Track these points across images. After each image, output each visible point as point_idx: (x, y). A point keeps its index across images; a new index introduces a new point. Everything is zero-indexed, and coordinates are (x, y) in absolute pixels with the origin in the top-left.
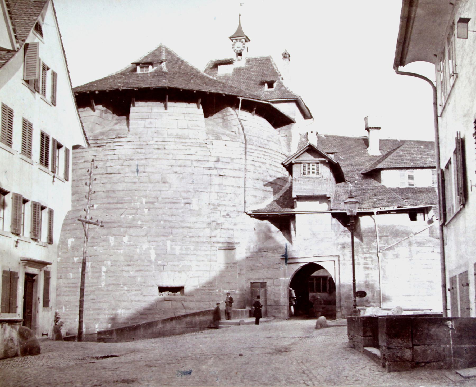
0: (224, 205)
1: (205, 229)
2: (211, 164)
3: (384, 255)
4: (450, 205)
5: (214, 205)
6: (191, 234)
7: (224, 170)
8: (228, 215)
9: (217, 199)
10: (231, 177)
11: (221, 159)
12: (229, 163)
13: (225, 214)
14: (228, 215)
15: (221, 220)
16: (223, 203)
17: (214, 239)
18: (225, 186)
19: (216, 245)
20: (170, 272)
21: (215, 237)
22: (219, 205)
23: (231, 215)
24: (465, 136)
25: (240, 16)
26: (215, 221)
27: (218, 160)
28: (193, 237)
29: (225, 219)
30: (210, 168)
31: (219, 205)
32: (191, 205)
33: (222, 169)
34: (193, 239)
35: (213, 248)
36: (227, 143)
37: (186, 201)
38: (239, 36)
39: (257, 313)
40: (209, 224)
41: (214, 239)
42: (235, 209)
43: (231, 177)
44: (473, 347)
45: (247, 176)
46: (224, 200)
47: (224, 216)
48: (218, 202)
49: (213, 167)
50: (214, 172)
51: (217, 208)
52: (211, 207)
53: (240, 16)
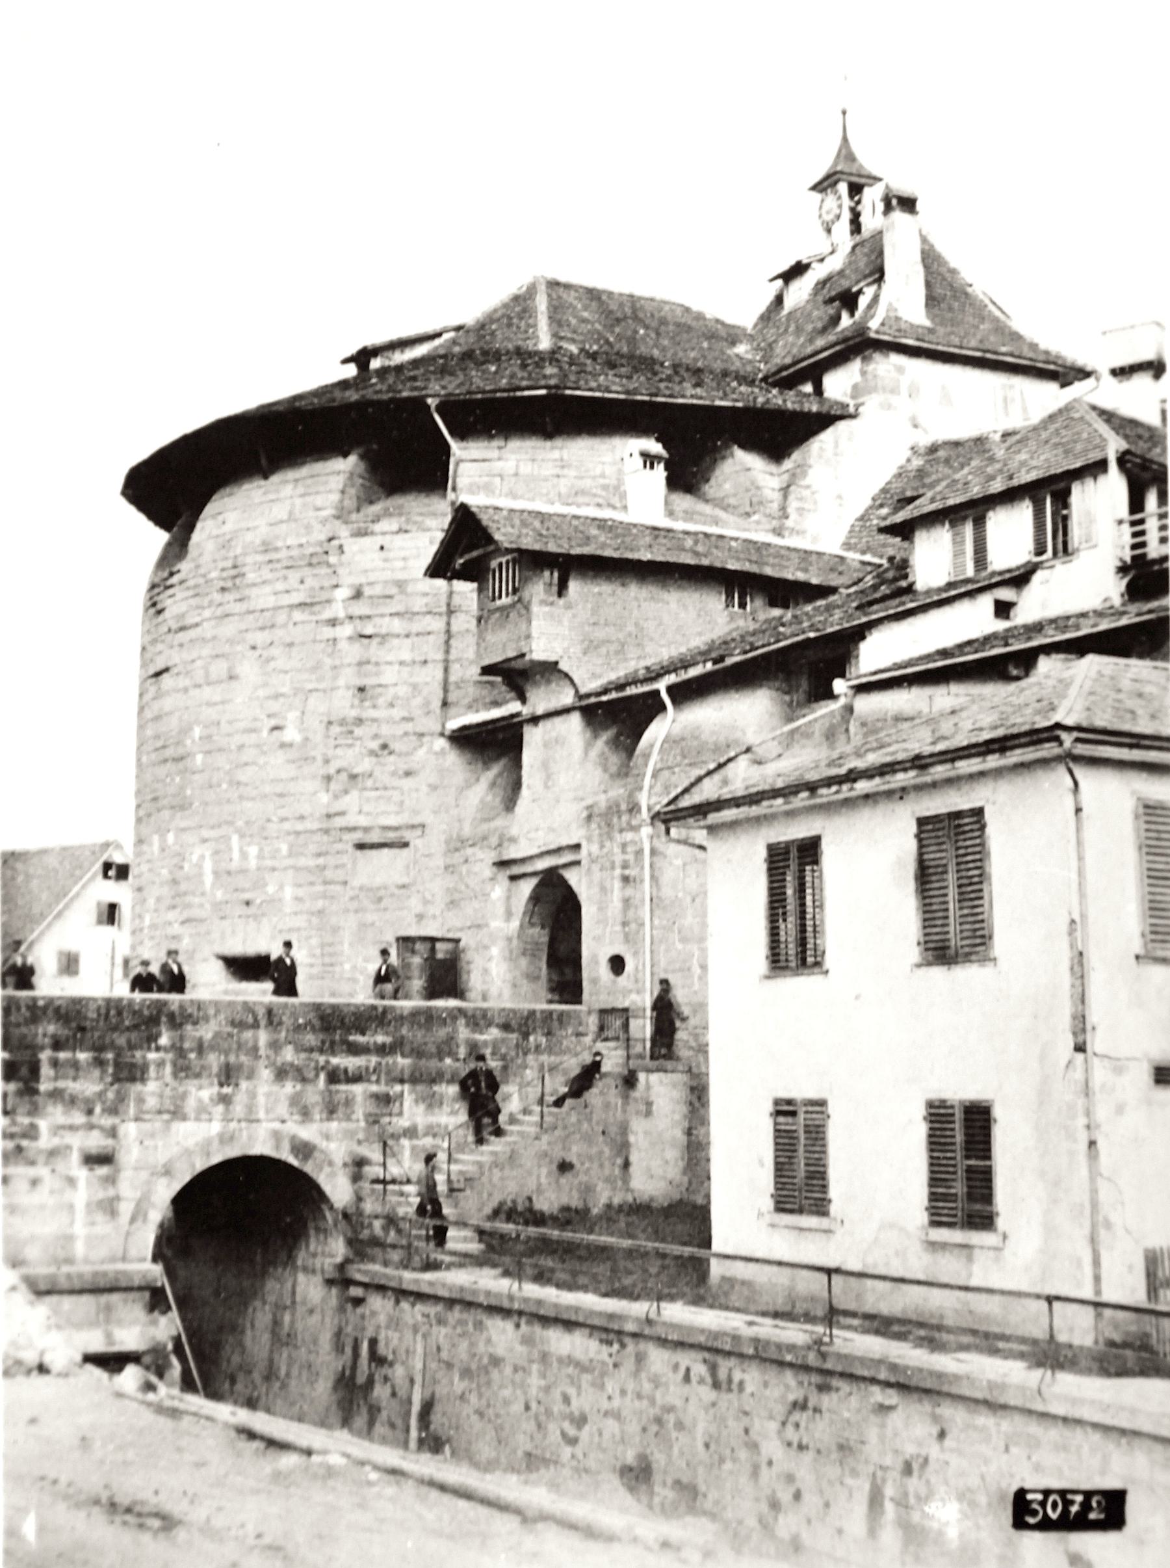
0: (374, 720)
1: (315, 793)
2: (338, 610)
5: (343, 722)
6: (283, 813)
7: (377, 620)
8: (384, 746)
11: (367, 591)
12: (390, 597)
13: (375, 745)
14: (384, 746)
15: (365, 765)
16: (372, 713)
17: (339, 822)
18: (377, 664)
20: (236, 920)
21: (342, 814)
22: (359, 721)
24: (346, 361)
25: (844, 113)
27: (358, 595)
29: (374, 759)
30: (333, 622)
31: (359, 721)
32: (286, 732)
33: (369, 617)
34: (287, 826)
36: (386, 540)
37: (273, 722)
38: (846, 180)
39: (1088, 1127)
41: (339, 822)
42: (409, 727)
44: (363, 1034)
45: (454, 628)
47: (373, 753)
50: (347, 630)
51: (351, 732)
52: (336, 729)
53: (844, 113)
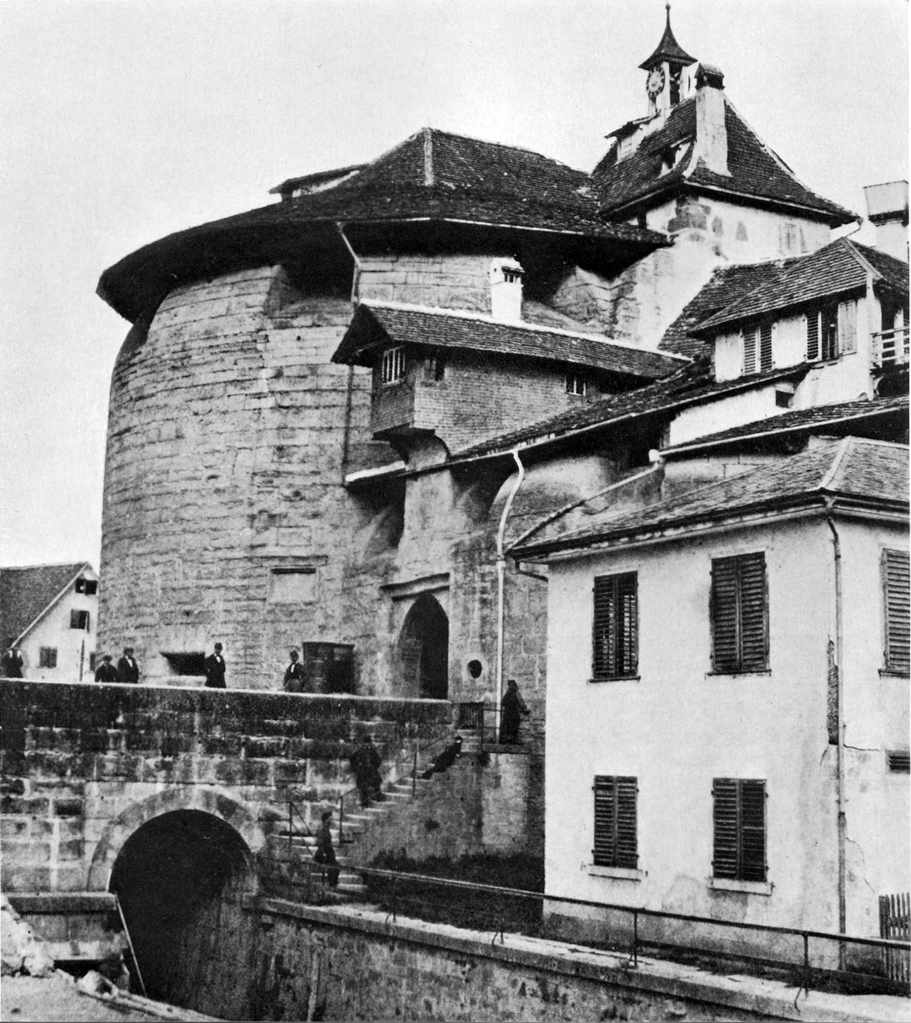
3: (336, 666)
4: (575, 351)
5: (264, 474)
8: (297, 494)
9: (273, 461)
10: (310, 407)
11: (286, 372)
13: (288, 492)
14: (297, 494)
17: (260, 552)
18: (293, 429)
19: (266, 564)
21: (263, 545)
22: (278, 474)
23: (306, 494)
25: (668, 8)
26: (266, 511)
27: (279, 375)
28: (220, 549)
31: (278, 474)
34: (220, 554)
35: (259, 571)
37: (210, 472)
38: (668, 57)
40: (252, 518)
41: (260, 552)
42: (317, 479)
43: (310, 407)
46: (290, 462)
48: (274, 467)
49: (266, 390)
50: (270, 402)
51: (271, 482)
52: (258, 480)
53: (668, 8)
